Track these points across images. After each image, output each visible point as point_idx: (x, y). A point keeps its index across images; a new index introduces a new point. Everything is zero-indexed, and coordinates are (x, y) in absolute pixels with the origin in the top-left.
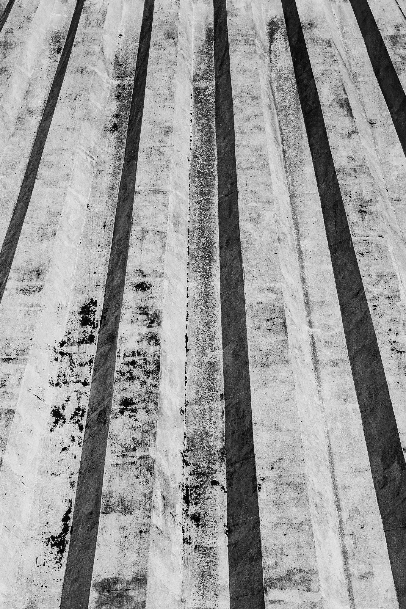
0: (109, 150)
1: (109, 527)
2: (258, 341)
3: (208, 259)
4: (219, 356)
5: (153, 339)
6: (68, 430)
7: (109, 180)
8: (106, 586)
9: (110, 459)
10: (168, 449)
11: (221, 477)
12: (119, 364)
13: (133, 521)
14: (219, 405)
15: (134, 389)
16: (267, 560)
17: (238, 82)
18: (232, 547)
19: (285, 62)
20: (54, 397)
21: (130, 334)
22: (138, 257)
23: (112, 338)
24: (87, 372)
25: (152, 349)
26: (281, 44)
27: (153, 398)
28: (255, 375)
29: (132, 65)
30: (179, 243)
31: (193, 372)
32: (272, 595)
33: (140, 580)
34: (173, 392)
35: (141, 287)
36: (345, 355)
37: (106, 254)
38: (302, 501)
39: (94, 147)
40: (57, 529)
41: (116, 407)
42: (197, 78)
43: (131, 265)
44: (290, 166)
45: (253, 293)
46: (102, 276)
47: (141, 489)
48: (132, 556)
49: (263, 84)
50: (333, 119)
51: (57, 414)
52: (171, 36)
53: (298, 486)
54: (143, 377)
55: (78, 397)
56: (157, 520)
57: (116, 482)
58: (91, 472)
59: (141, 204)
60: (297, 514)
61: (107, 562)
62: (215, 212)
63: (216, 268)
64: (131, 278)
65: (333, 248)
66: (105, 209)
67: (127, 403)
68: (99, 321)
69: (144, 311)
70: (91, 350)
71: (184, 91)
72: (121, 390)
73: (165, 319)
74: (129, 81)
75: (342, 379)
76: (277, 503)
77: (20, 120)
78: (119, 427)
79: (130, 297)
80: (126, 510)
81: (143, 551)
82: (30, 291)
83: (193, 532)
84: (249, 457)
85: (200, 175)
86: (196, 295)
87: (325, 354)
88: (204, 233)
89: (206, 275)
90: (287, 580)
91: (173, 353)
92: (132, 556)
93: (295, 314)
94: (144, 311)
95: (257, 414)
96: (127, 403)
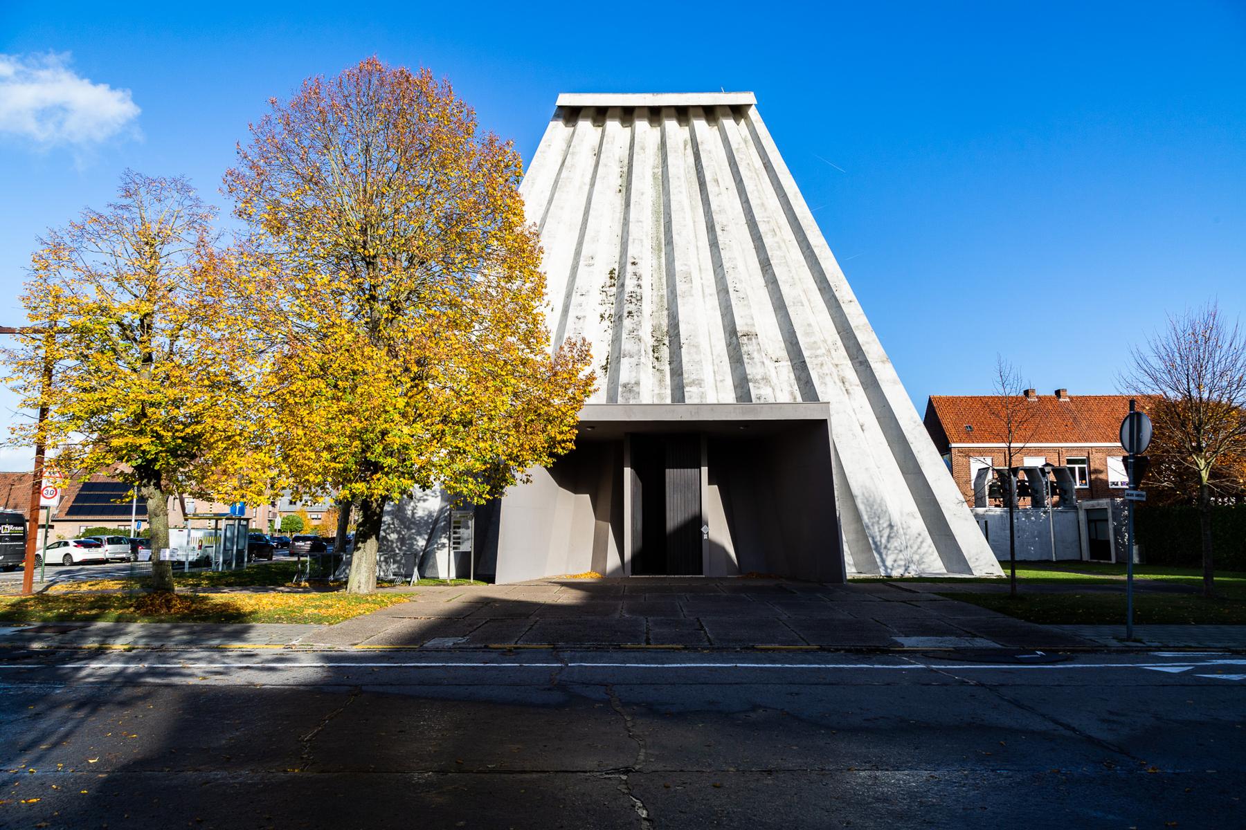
0: (619, 201)
1: (625, 362)
2: (681, 287)
3: (660, 251)
4: (665, 292)
5: (639, 286)
6: (607, 323)
7: (619, 215)
8: (625, 386)
9: (624, 336)
10: (646, 332)
11: (667, 342)
12: (626, 297)
13: (634, 360)
14: (665, 313)
15: (632, 307)
16: (685, 376)
17: (672, 170)
18: (671, 370)
19: (691, 160)
20: (601, 310)
21: (630, 284)
22: (632, 251)
23: (623, 285)
24: (612, 299)
25: (638, 290)
26: (690, 151)
27: (639, 311)
28: (679, 300)
29: (626, 162)
30: (648, 243)
31: (656, 299)
32: (687, 389)
33: (637, 383)
34: (647, 307)
35: (634, 263)
36: (715, 291)
37: (618, 249)
38: (698, 352)
39: (591, 378)
40: (604, 363)
41: (626, 314)
42: (654, 168)
43: (630, 254)
44: (693, 208)
45: (679, 266)
46: (617, 258)
47: (636, 348)
48: (634, 374)
49: (682, 171)
50: (711, 187)
51: (602, 316)
52: (643, 148)
53: (697, 346)
54: (490, 290)
55: (610, 310)
56: (643, 360)
57: (627, 345)
58: (616, 340)
59: (632, 226)
60: (697, 358)
61: (625, 376)
62: (662, 229)
63: (663, 254)
64: (630, 260)
65: (711, 246)
66: (618, 229)
67: (630, 313)
68: (617, 277)
69: (635, 274)
70: (614, 289)
71: (649, 179)
72: (628, 307)
73: (643, 278)
74: (625, 169)
75: (714, 302)
76: (689, 353)
77: (580, 188)
78: (627, 323)
79: (630, 268)
80: (631, 356)
81: (638, 372)
82: (590, 265)
83: (656, 364)
84: (678, 335)
85: (656, 212)
86: (655, 266)
87: (707, 291)
88: (658, 238)
89: (659, 257)
90: (692, 383)
91: (647, 292)
92: (634, 374)
93: (695, 275)
94: (635, 274)
95: (681, 317)
96: (630, 313)
